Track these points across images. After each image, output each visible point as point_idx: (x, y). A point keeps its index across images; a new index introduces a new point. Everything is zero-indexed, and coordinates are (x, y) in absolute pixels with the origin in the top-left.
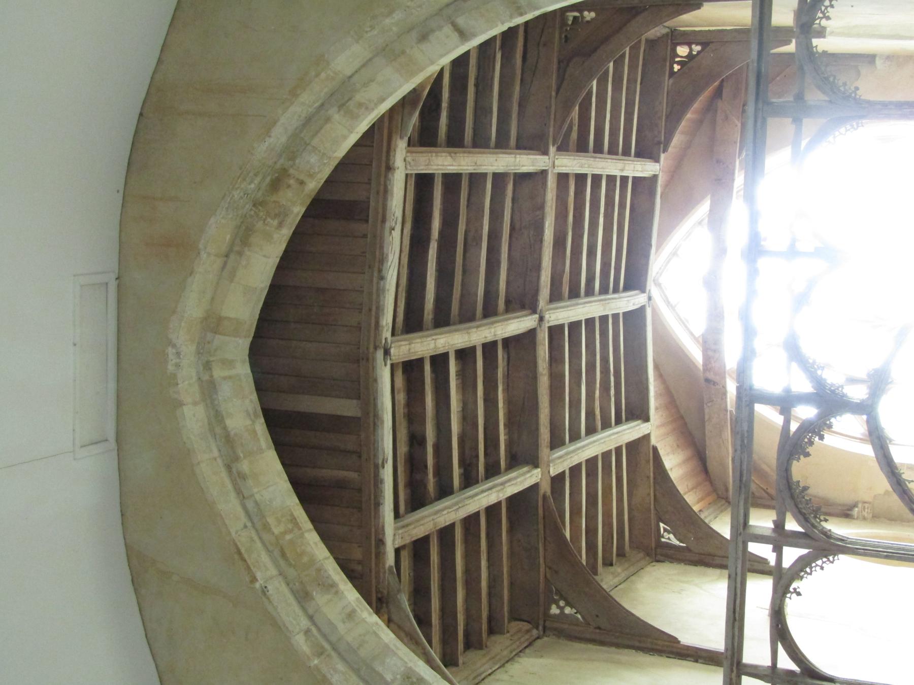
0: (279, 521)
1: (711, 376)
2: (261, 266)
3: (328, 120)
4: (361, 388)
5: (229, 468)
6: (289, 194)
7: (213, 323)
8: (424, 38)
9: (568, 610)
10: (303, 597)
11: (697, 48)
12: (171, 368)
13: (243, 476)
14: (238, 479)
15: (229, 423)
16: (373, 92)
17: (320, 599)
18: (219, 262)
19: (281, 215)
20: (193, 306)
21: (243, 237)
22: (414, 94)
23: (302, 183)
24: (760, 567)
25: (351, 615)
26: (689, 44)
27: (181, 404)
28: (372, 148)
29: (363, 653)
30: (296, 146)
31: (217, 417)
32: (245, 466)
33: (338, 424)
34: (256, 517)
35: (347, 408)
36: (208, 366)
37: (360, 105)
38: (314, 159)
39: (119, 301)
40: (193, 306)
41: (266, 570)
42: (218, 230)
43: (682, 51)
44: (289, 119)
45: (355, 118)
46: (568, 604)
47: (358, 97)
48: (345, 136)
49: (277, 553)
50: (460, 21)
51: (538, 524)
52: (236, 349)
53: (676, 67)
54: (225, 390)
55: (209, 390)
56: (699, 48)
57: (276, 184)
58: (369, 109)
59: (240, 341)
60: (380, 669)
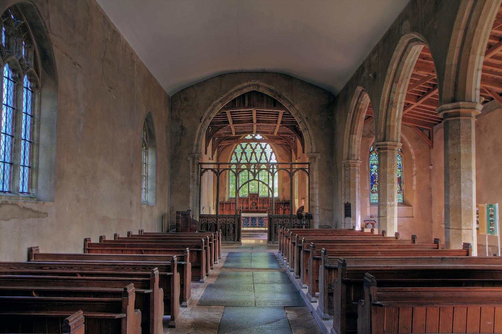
0: (231, 97)
1: (239, 140)
2: (267, 93)
3: (288, 104)
4: (249, 106)
5: (238, 89)
6: (278, 98)
7: (259, 86)
8: (299, 117)
9: (210, 129)
10: (221, 101)
11: (307, 170)
12: (252, 81)
13: (237, 91)
14: (237, 91)
15: (245, 89)
16: (292, 110)
17: (221, 104)
18: (268, 87)
19: (275, 96)
21: (272, 91)
22: (291, 114)
23: (279, 99)
24: (213, 154)
25: (219, 108)
26: (295, 139)
27: (247, 82)
28: (284, 108)
29: (214, 111)
30: (284, 99)
31: (245, 87)
32: (239, 92)
33: (244, 104)
34: (231, 94)
36: (253, 85)
37: (290, 108)
38: (283, 101)
39: (261, 72)
40: (261, 84)
41: (224, 96)
42: (273, 88)
43: (294, 138)
44: (288, 98)
45: (289, 107)
46: (211, 130)
47: (291, 108)
48: (286, 105)
49: (227, 97)
50: (302, 123)
51: (285, 161)
53: (291, 137)
54: (249, 88)
55: (249, 86)
56: (308, 171)
57: (279, 96)
58: (290, 109)
59: (343, 228)
60: (212, 114)
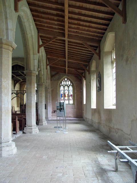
7: (18, 63)
20: (18, 62)
35: (15, 70)
40: (18, 62)
52: (17, 64)
